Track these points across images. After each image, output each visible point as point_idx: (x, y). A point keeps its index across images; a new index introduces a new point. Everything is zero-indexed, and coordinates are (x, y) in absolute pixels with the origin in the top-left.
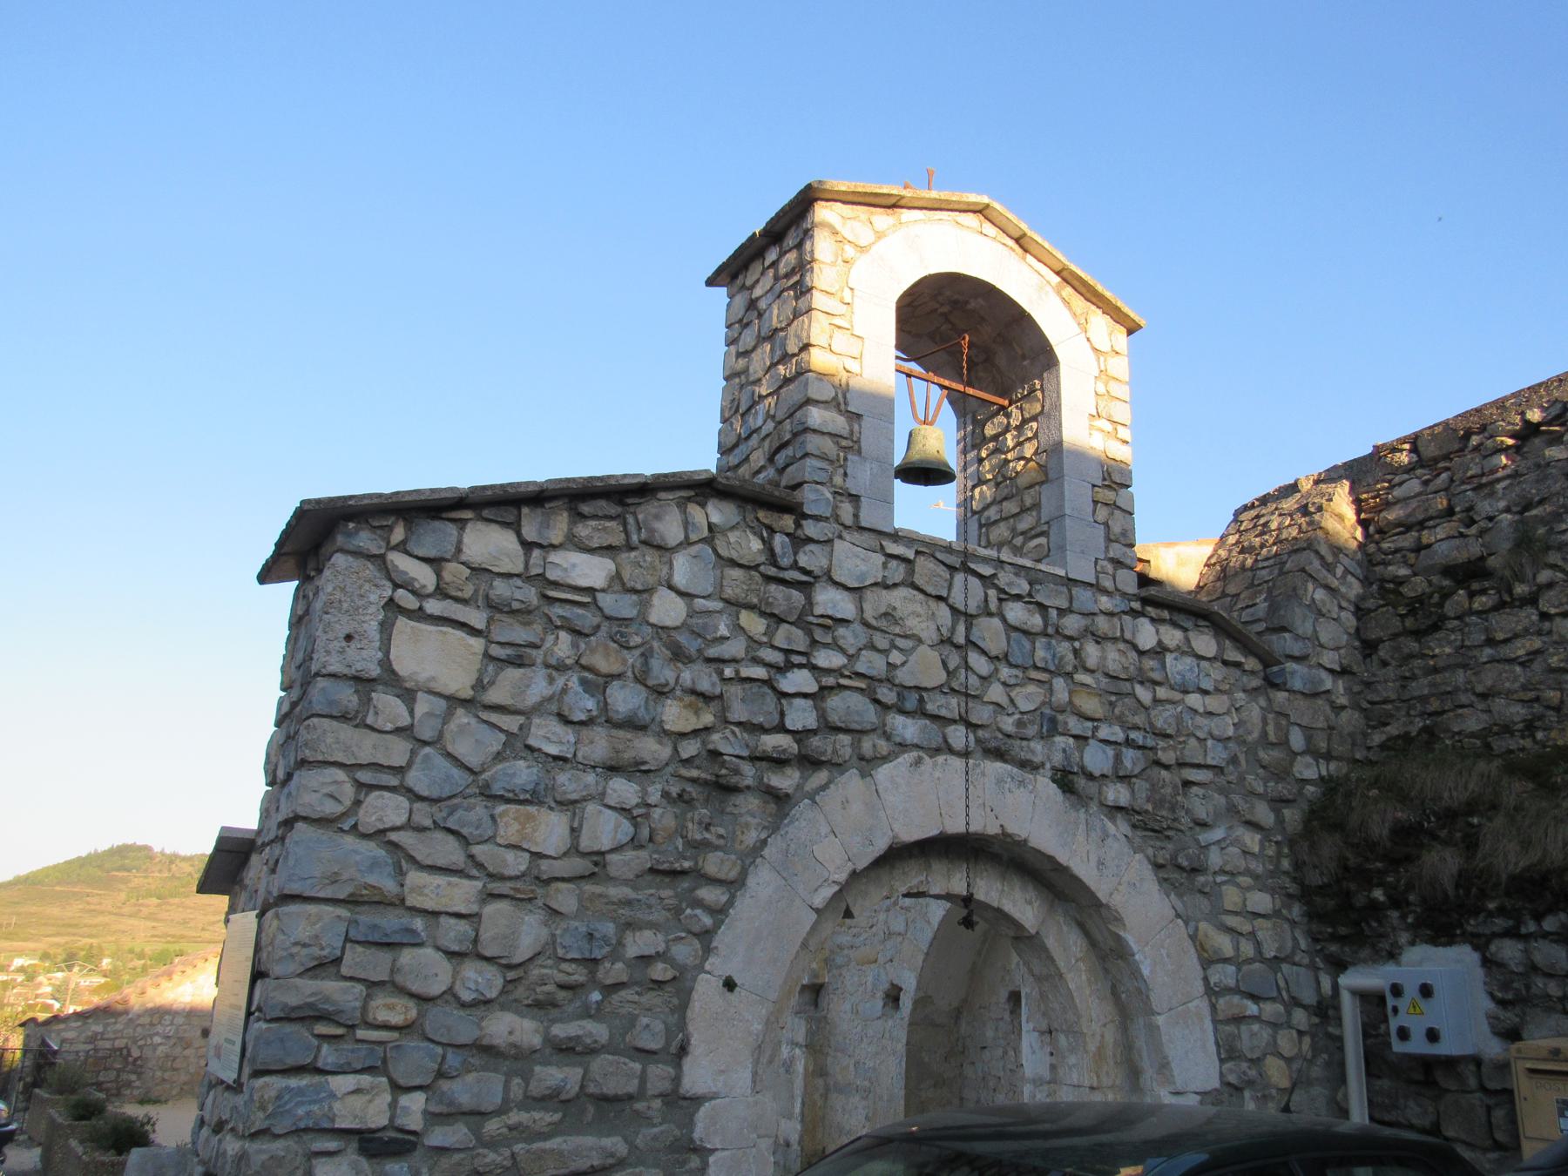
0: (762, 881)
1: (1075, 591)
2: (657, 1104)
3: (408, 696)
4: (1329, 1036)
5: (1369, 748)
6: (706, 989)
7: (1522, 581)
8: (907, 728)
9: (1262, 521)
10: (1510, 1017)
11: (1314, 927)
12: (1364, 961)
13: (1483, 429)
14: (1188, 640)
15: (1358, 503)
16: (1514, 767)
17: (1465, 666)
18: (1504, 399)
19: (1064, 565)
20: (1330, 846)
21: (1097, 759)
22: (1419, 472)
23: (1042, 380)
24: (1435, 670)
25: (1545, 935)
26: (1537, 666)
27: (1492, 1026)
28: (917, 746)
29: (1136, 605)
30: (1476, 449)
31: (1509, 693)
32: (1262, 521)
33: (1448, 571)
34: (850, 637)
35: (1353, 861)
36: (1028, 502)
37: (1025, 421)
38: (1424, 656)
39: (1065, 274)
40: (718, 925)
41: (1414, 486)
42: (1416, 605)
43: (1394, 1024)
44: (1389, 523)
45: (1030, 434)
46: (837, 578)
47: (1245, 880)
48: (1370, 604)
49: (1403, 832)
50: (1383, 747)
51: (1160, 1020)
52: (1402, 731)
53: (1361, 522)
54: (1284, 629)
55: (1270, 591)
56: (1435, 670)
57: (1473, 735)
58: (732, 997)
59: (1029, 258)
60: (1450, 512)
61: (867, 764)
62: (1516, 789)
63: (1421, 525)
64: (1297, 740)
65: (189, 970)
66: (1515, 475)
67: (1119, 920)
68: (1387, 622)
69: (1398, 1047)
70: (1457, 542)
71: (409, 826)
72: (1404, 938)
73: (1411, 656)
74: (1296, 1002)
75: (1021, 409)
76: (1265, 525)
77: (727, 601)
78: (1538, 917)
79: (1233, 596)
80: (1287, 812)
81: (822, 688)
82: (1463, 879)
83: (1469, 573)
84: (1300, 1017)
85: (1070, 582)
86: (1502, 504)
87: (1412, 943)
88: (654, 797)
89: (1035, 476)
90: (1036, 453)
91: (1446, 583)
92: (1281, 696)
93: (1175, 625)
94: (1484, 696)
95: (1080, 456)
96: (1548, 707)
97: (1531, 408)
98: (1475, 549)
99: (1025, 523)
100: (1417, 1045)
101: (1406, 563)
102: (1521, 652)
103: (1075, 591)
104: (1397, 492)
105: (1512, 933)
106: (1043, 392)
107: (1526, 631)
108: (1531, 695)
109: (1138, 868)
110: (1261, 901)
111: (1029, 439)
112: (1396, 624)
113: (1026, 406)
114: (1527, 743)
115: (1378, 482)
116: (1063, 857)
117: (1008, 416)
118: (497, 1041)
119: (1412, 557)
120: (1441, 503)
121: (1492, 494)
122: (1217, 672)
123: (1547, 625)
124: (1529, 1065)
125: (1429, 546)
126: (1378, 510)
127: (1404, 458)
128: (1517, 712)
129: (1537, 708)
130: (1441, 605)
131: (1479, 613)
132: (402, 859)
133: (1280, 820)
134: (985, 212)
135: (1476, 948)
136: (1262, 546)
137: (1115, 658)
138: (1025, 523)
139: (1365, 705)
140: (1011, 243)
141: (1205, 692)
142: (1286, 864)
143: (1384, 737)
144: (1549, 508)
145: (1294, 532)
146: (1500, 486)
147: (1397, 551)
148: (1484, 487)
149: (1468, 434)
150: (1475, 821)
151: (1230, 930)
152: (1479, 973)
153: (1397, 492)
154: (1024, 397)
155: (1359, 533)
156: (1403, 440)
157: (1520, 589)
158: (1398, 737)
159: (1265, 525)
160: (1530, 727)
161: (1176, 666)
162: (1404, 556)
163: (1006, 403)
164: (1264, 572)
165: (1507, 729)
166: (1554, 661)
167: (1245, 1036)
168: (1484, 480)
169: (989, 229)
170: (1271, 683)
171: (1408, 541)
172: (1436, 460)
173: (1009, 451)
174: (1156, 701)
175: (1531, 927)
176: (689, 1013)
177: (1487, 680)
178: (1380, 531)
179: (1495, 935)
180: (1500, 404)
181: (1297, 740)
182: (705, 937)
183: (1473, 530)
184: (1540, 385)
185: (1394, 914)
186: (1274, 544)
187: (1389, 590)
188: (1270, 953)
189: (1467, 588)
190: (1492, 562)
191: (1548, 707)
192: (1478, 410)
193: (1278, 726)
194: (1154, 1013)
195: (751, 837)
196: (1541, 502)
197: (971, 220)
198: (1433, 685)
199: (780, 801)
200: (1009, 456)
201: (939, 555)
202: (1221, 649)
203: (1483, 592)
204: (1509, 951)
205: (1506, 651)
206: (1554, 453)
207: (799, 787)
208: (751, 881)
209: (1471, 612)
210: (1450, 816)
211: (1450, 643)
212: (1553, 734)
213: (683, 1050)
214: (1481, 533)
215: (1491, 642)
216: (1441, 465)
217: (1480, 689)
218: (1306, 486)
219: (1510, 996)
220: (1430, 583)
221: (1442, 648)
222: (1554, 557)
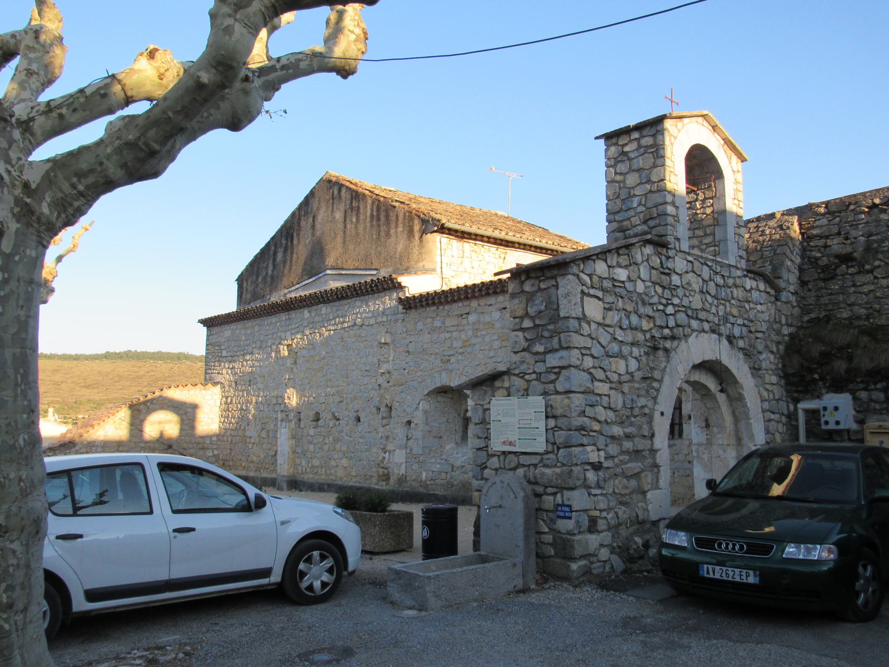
0: (666, 379)
1: (732, 269)
2: (648, 452)
3: (589, 323)
4: (792, 425)
5: (802, 322)
6: (657, 415)
7: (868, 264)
8: (695, 324)
9: (761, 229)
10: (861, 416)
11: (789, 388)
12: (808, 399)
13: (856, 203)
14: (757, 285)
15: (800, 225)
16: (864, 332)
17: (843, 294)
18: (866, 193)
19: (728, 259)
20: (796, 359)
21: (737, 331)
22: (828, 216)
23: (715, 183)
24: (831, 294)
25: (877, 389)
26: (871, 296)
27: (854, 419)
28: (697, 330)
29: (745, 273)
30: (852, 210)
31: (859, 305)
32: (761, 229)
33: (837, 256)
34: (680, 292)
35: (806, 364)
36: (708, 232)
37: (705, 199)
38: (826, 288)
39: (726, 140)
40: (658, 394)
41: (824, 221)
42: (825, 268)
43: (823, 420)
44: (813, 235)
45: (709, 205)
46: (677, 271)
47: (770, 372)
48: (806, 267)
49: (823, 354)
50: (808, 321)
51: (752, 421)
52: (816, 316)
53: (801, 233)
54: (780, 278)
55: (771, 261)
56: (831, 294)
57: (845, 319)
58: (662, 418)
59: (716, 134)
60: (839, 234)
61: (687, 337)
62: (865, 339)
63: (827, 237)
64: (783, 321)
65: (101, 422)
66: (867, 223)
67: (742, 388)
68: (812, 274)
69: (824, 427)
70: (842, 246)
71: (594, 367)
72: (824, 391)
73: (822, 288)
74: (783, 414)
75: (704, 193)
76: (763, 231)
77: (652, 282)
78: (875, 384)
79: (753, 261)
80: (780, 347)
81: (676, 311)
82: (848, 371)
83: (846, 259)
84: (784, 419)
85: (730, 266)
86: (861, 233)
87: (827, 393)
88: (642, 353)
89: (711, 222)
90: (713, 212)
91: (836, 261)
92: (779, 303)
93: (754, 279)
94: (850, 305)
95: (732, 213)
96: (875, 311)
97: (876, 198)
98: (849, 249)
99: (708, 240)
100: (832, 426)
101: (819, 251)
102: (866, 290)
103: (732, 269)
104: (817, 223)
105: (865, 389)
106: (716, 188)
107: (868, 283)
108: (869, 306)
109: (746, 369)
110: (774, 379)
111: (708, 206)
112: (816, 276)
113: (707, 192)
114: (866, 323)
115: (809, 218)
116: (730, 367)
117: (697, 195)
118: (616, 435)
119: (823, 249)
120: (835, 230)
121: (857, 228)
122: (764, 295)
123: (876, 281)
124: (871, 431)
125: (830, 246)
126: (809, 229)
127: (822, 210)
128: (863, 311)
129: (871, 311)
130: (835, 269)
131: (850, 274)
132: (593, 379)
133: (778, 350)
134: (706, 117)
135: (851, 394)
136: (764, 241)
137: (738, 293)
138: (708, 240)
139: (802, 306)
140: (710, 128)
141: (761, 304)
142: (780, 366)
143: (809, 318)
144: (879, 237)
145: (778, 236)
146: (861, 226)
147: (816, 246)
148: (854, 226)
149: (850, 204)
150: (850, 350)
151: (767, 390)
152: (851, 402)
153: (817, 223)
154: (705, 188)
155: (800, 237)
156: (822, 203)
157: (867, 267)
158: (815, 318)
159: (763, 231)
160: (868, 317)
161: (755, 295)
162: (819, 249)
163: (696, 189)
164: (767, 253)
165: (859, 318)
166: (878, 294)
167: (771, 426)
168: (854, 223)
169: (705, 123)
170: (777, 299)
171: (821, 242)
172: (835, 212)
173: (697, 209)
174: (750, 308)
175: (873, 387)
176: (653, 423)
177: (852, 299)
178: (808, 237)
179: (858, 390)
180: (863, 194)
181: (783, 321)
182: (655, 399)
183: (849, 242)
184: (880, 189)
185: (821, 383)
186: (769, 241)
187: (814, 262)
188: (777, 397)
189: (846, 265)
190: (855, 255)
191: (875, 311)
192: (854, 196)
193: (779, 316)
194: (750, 419)
195: (664, 364)
196: (877, 234)
197: (700, 119)
198: (830, 299)
199: (666, 350)
200: (698, 212)
201: (700, 260)
202: (765, 288)
203: (852, 267)
204: (863, 395)
205: (860, 289)
206: (884, 216)
207: (671, 347)
208: (665, 380)
209: (847, 274)
210: (841, 349)
211: (838, 285)
212: (876, 320)
213: (653, 435)
214: (852, 243)
215: (854, 285)
216: (837, 214)
217: (849, 302)
218: (778, 216)
219: (861, 409)
220: (829, 261)
221: (835, 286)
222: (880, 256)
